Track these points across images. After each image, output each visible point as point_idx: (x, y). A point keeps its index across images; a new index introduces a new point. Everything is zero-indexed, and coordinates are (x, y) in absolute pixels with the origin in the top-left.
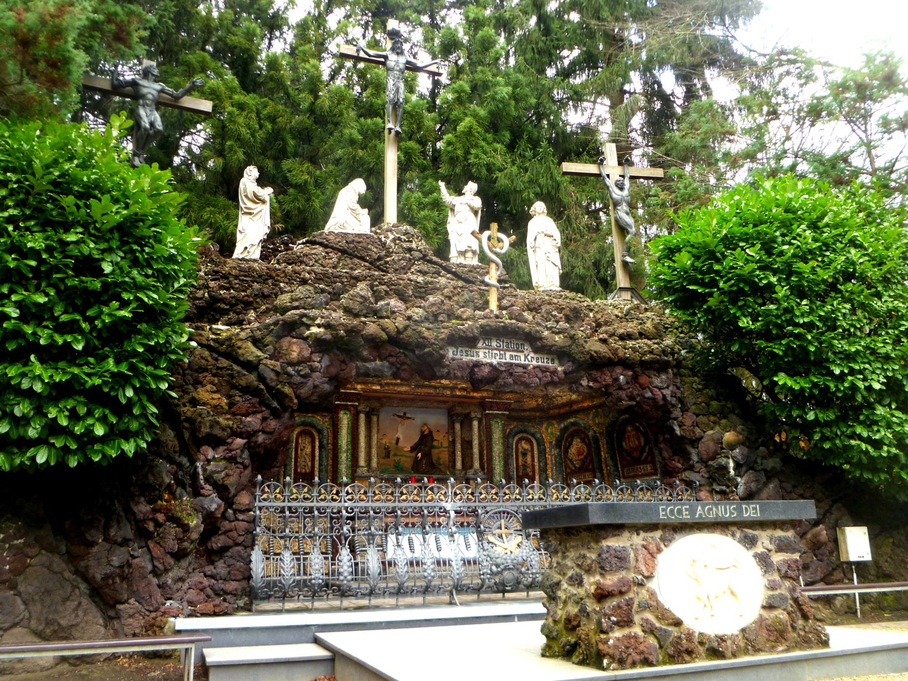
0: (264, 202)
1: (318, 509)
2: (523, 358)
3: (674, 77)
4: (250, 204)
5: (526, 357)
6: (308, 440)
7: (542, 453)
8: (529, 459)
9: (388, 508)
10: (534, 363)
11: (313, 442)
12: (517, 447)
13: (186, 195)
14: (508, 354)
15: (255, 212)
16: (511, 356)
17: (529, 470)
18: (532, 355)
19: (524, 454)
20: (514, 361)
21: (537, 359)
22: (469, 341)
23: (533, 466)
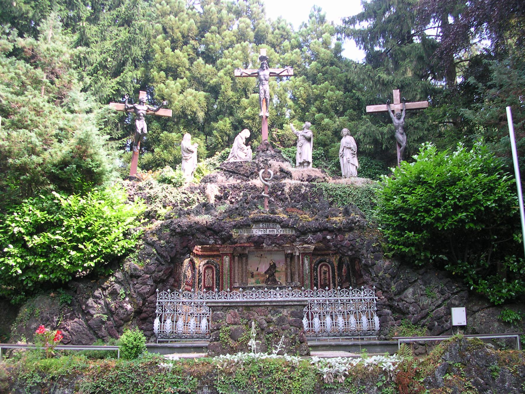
0: (193, 152)
1: (340, 300)
2: (276, 231)
3: (355, 43)
4: (186, 155)
5: (277, 231)
6: (210, 271)
7: (333, 272)
8: (322, 277)
9: (335, 300)
10: (282, 233)
11: (213, 271)
12: (320, 269)
13: (201, 120)
14: (268, 230)
15: (188, 158)
16: (270, 231)
17: (327, 281)
18: (281, 229)
19: (325, 273)
20: (271, 233)
21: (283, 231)
22: (247, 226)
23: (329, 279)
